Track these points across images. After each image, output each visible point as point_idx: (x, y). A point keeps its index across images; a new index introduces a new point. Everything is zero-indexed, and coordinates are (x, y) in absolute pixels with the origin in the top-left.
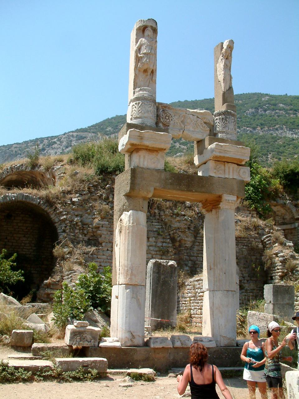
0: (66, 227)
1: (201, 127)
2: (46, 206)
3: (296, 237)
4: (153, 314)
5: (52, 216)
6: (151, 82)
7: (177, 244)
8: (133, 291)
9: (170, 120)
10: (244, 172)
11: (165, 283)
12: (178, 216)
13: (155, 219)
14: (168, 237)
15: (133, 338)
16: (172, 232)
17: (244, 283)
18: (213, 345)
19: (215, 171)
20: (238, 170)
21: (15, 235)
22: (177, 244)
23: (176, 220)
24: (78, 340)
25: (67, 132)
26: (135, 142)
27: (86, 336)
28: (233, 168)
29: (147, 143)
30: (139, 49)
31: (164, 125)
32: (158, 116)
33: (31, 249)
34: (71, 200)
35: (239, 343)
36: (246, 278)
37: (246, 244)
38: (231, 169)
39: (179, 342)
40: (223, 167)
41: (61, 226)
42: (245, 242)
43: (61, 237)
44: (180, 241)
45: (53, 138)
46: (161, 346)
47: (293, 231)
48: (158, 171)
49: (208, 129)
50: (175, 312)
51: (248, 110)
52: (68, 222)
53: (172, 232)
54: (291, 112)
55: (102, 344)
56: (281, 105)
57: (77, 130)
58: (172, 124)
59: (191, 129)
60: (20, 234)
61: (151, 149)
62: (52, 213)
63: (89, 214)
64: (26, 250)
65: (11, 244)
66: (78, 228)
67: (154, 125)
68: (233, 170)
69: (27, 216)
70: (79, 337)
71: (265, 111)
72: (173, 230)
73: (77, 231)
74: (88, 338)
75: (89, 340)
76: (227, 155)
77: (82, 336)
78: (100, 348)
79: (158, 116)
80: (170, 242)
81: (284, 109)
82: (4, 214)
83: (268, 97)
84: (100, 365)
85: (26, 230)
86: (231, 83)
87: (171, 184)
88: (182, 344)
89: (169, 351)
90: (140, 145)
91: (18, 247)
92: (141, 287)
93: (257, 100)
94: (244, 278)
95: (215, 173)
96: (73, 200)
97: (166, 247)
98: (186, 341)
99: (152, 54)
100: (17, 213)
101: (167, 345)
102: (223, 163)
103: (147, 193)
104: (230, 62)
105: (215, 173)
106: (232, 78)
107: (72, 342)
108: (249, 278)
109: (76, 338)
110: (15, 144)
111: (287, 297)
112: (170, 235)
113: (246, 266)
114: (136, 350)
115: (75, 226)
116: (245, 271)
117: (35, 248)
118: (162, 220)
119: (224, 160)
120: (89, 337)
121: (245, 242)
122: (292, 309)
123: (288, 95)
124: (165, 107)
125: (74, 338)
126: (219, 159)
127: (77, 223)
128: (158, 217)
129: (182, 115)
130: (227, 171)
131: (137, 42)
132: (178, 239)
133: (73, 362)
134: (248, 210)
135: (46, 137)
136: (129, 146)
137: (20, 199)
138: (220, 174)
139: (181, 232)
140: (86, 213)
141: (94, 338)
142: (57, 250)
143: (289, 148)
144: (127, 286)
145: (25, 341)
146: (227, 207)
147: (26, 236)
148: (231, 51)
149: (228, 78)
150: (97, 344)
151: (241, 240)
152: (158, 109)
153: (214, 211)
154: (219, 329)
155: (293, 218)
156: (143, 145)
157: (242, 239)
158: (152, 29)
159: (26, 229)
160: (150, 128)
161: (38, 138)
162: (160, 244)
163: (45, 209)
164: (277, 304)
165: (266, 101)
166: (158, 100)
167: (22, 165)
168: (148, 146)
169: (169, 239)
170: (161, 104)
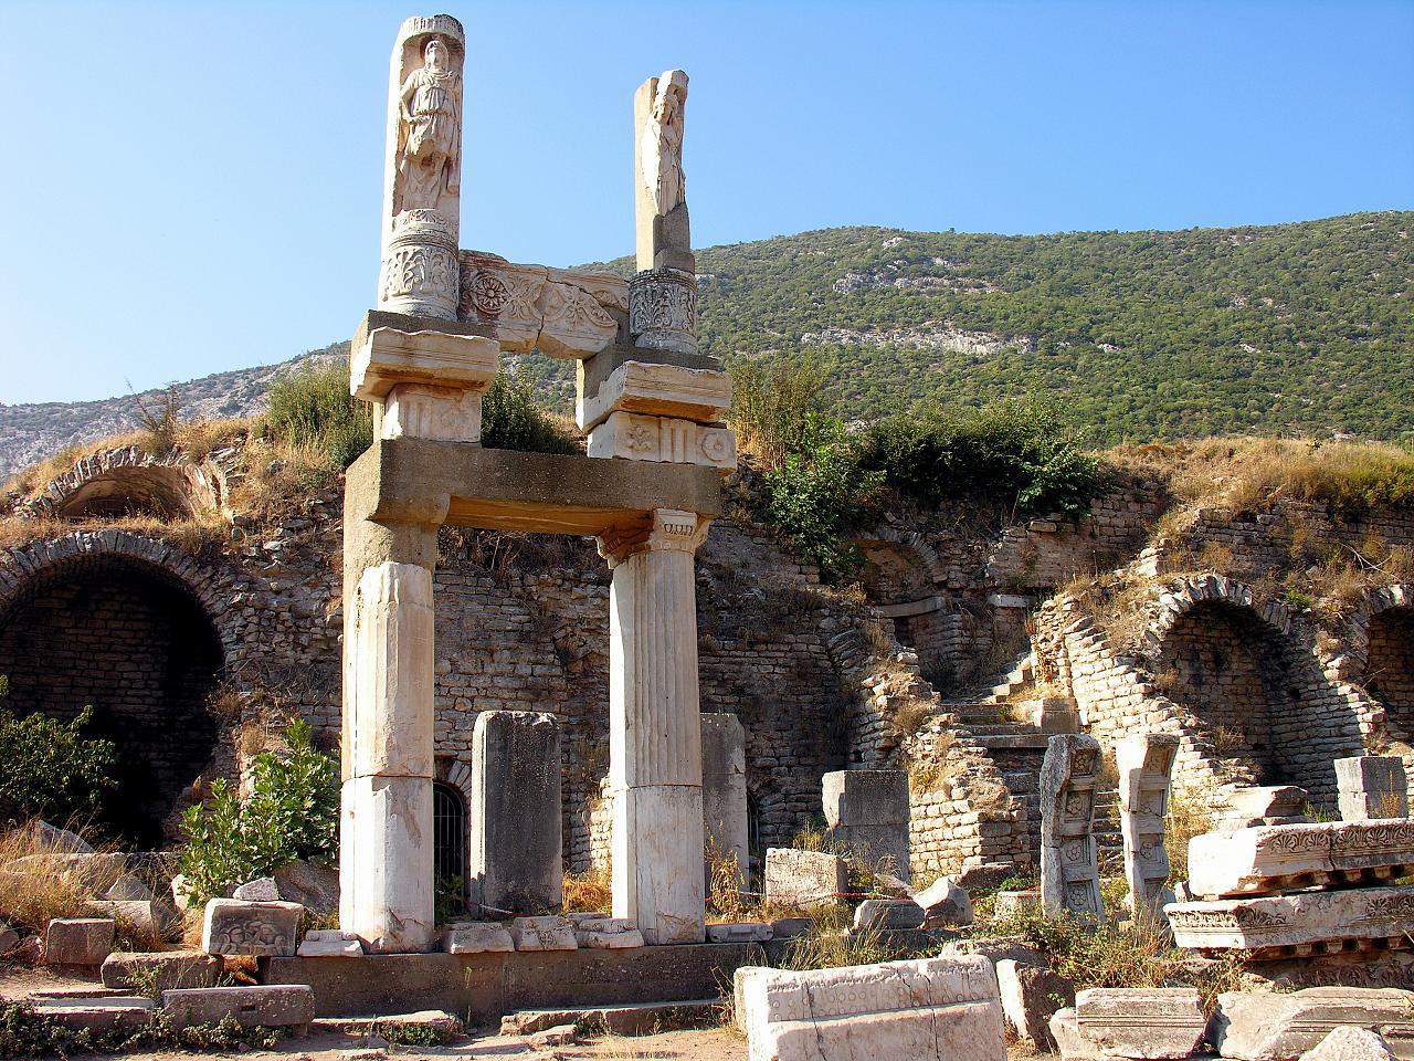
0: (245, 627)
1: (593, 318)
3: (939, 636)
5: (204, 597)
6: (444, 192)
7: (578, 667)
8: (395, 794)
12: (577, 586)
15: (398, 929)
18: (634, 940)
19: (630, 442)
20: (701, 438)
21: (98, 657)
22: (578, 667)
24: (236, 939)
25: (302, 351)
27: (259, 927)
28: (685, 431)
29: (425, 365)
30: (409, 100)
32: (464, 289)
33: (151, 696)
34: (261, 546)
37: (781, 661)
40: (654, 430)
41: (233, 623)
42: (778, 654)
43: (231, 656)
44: (585, 658)
45: (262, 372)
48: (461, 447)
50: (559, 860)
52: (251, 610)
54: (966, 281)
55: (306, 949)
56: (938, 261)
59: (564, 324)
60: (116, 652)
62: (203, 586)
64: (135, 699)
65: (87, 683)
66: (280, 627)
68: (685, 437)
74: (266, 931)
75: (270, 938)
76: (663, 396)
77: (247, 927)
81: (948, 273)
83: (899, 239)
85: (134, 642)
86: (681, 192)
88: (542, 940)
90: (408, 374)
91: (110, 692)
92: (417, 782)
93: (870, 247)
94: (778, 759)
95: (632, 447)
97: (544, 676)
98: (554, 933)
101: (498, 946)
102: (656, 418)
103: (431, 509)
104: (679, 133)
105: (632, 447)
107: (217, 945)
108: (793, 760)
109: (230, 934)
111: (888, 804)
112: (554, 640)
114: (407, 961)
116: (782, 738)
117: (160, 693)
121: (778, 654)
126: (641, 409)
127: (278, 614)
128: (519, 589)
130: (667, 440)
131: (403, 82)
135: (241, 372)
136: (376, 379)
137: (108, 547)
140: (305, 584)
141: (284, 933)
142: (226, 701)
143: (963, 386)
144: (378, 780)
145: (89, 949)
148: (681, 103)
149: (672, 177)
150: (290, 948)
151: (767, 650)
152: (463, 269)
155: (928, 582)
156: (419, 374)
158: (447, 45)
160: (439, 324)
162: (525, 670)
170: (474, 254)
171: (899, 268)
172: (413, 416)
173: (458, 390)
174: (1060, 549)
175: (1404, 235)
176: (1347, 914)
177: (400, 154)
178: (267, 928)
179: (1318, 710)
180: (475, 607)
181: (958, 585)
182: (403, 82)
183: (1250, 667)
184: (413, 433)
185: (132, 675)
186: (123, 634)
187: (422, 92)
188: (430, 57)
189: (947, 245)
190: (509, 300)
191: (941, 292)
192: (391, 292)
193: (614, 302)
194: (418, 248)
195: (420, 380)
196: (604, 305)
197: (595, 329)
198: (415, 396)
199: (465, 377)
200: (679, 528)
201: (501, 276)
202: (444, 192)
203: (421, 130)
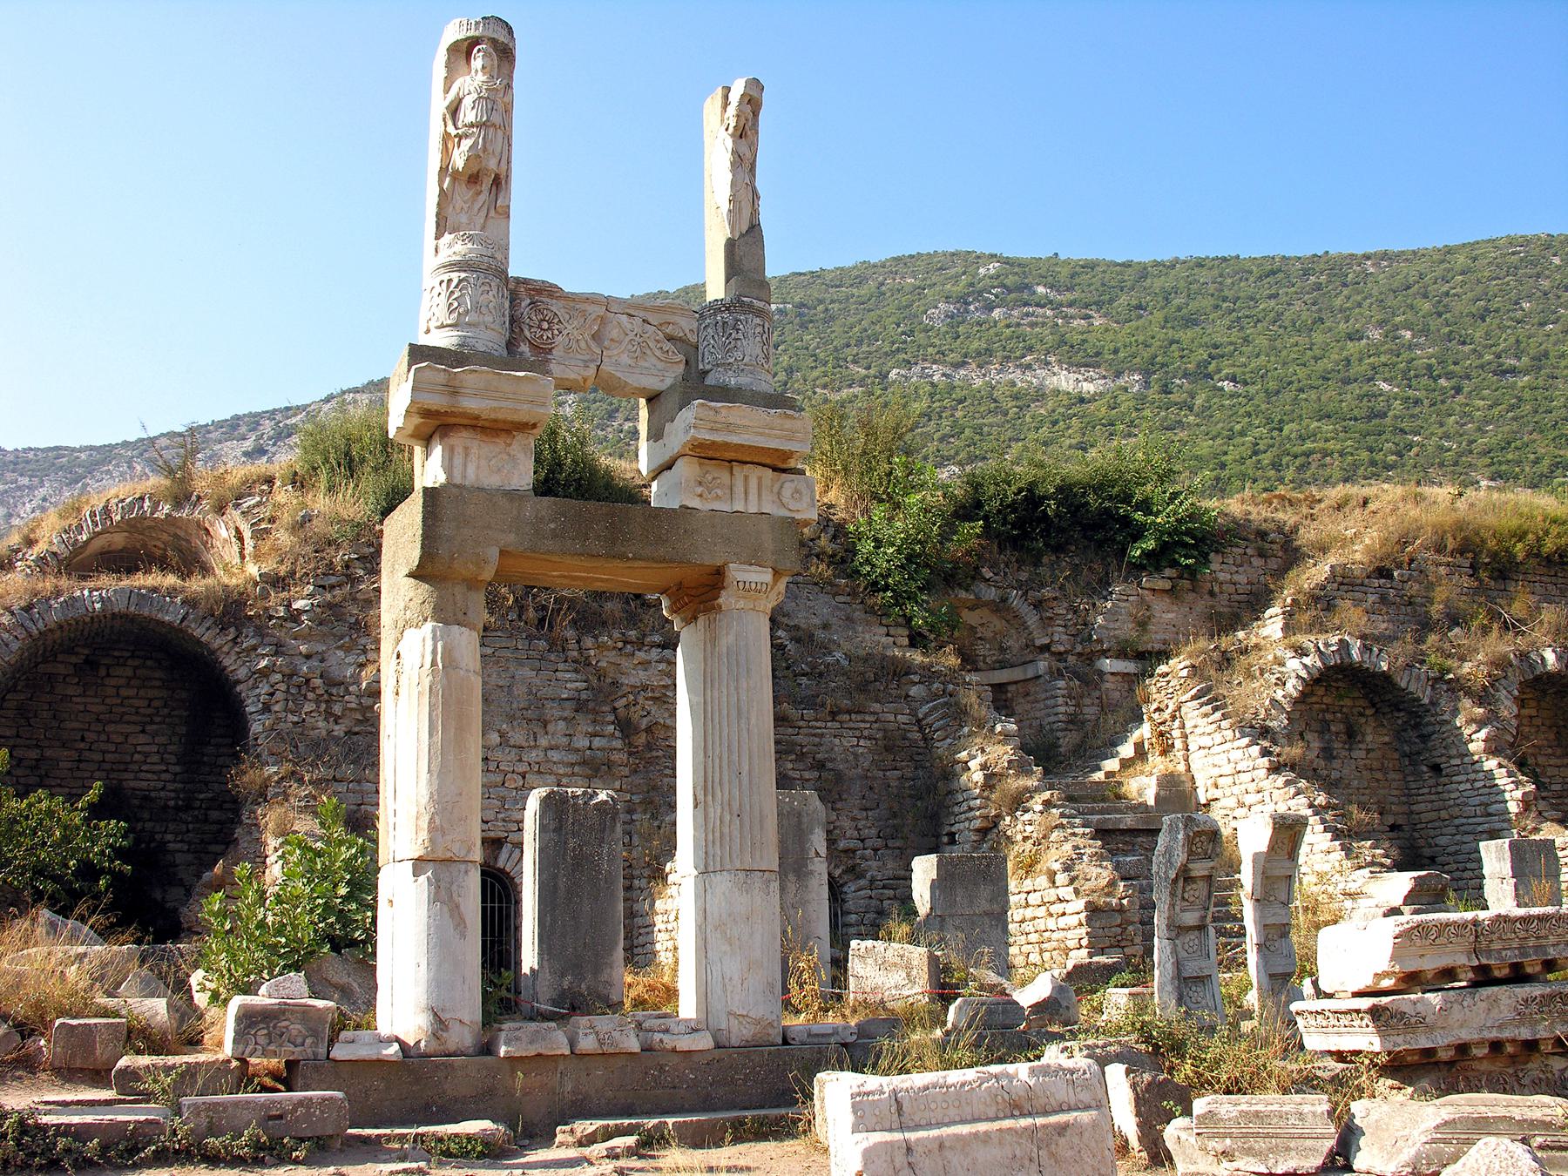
0: (272, 694)
1: (658, 353)
2: (208, 629)
4: (545, 963)
6: (492, 213)
7: (641, 739)
9: (556, 332)
10: (797, 491)
11: (580, 862)
13: (566, 661)
14: (611, 718)
16: (623, 701)
17: (863, 858)
19: (699, 490)
21: (110, 728)
22: (641, 739)
23: (636, 662)
24: (262, 1040)
25: (335, 390)
26: (436, 402)
27: (287, 1027)
28: (760, 479)
29: (470, 404)
30: (454, 110)
31: (534, 347)
34: (289, 606)
35: (790, 1035)
36: (868, 843)
37: (866, 733)
38: (753, 483)
39: (592, 1037)
40: (725, 477)
42: (862, 725)
43: (256, 728)
44: (648, 730)
45: (291, 412)
46: (532, 1051)
47: (1032, 688)
49: (681, 357)
50: (619, 953)
51: (936, 307)
52: (278, 677)
53: (623, 701)
54: (1071, 311)
55: (339, 1052)
56: (1041, 290)
57: (371, 383)
58: (561, 347)
59: (625, 359)
60: (128, 723)
61: (487, 424)
62: (226, 649)
63: (348, 650)
64: (149, 776)
65: (98, 757)
66: (310, 695)
67: (500, 349)
69: (149, 663)
70: (265, 1031)
71: (990, 308)
72: (624, 696)
73: (308, 707)
74: (294, 1032)
76: (734, 439)
77: (275, 1027)
78: (333, 1064)
79: (513, 320)
80: (617, 734)
81: (1051, 302)
82: (74, 659)
84: (322, 1112)
85: (149, 711)
86: (755, 212)
87: (555, 535)
88: (601, 1042)
89: (561, 1067)
90: (453, 414)
91: (122, 767)
92: (463, 867)
94: (862, 841)
95: (701, 496)
96: (294, 607)
98: (614, 1034)
99: (494, 125)
100: (116, 653)
104: (753, 147)
105: (701, 496)
106: (759, 198)
107: (241, 1047)
109: (255, 1035)
110: (163, 435)
111: (985, 891)
113: (868, 805)
114: (451, 1065)
115: (303, 692)
117: (178, 769)
118: (590, 664)
119: (729, 455)
120: (296, 1028)
122: (999, 930)
123: (1062, 257)
124: (539, 291)
125: (248, 1033)
126: (711, 454)
127: (308, 681)
128: (575, 653)
129: (593, 316)
131: (447, 91)
132: (644, 723)
133: (236, 1104)
134: (881, 624)
136: (417, 420)
137: (120, 607)
138: (718, 497)
139: (652, 698)
141: (315, 1033)
142: (249, 777)
145: (98, 1052)
146: (741, 604)
147: (149, 728)
148: (756, 114)
150: (322, 1050)
152: (514, 299)
153: (702, 619)
154: (725, 991)
156: (464, 415)
157: (853, 716)
159: (149, 706)
160: (487, 359)
161: (240, 413)
163: (203, 639)
164: (951, 916)
165: (991, 277)
166: (513, 272)
167: (142, 499)
168: (477, 418)
169: (613, 723)
170: (526, 281)
171: (997, 296)
172: (458, 461)
173: (508, 432)
174: (1175, 608)
175: (1557, 261)
176: (1494, 1013)
177: (443, 171)
178: (296, 1028)
179: (1462, 787)
180: (527, 672)
181: (1062, 649)
182: (447, 91)
183: (1387, 739)
184: (458, 480)
185: (147, 749)
186: (136, 702)
187: (467, 102)
188: (477, 62)
189: (1049, 270)
190: (565, 332)
191: (1044, 324)
192: (433, 324)
193: (681, 334)
194: (463, 275)
195: (465, 422)
196: (670, 338)
197: (660, 365)
198: (460, 439)
199: (516, 418)
200: (753, 586)
201: (556, 306)
202: (492, 213)
203: (466, 144)
